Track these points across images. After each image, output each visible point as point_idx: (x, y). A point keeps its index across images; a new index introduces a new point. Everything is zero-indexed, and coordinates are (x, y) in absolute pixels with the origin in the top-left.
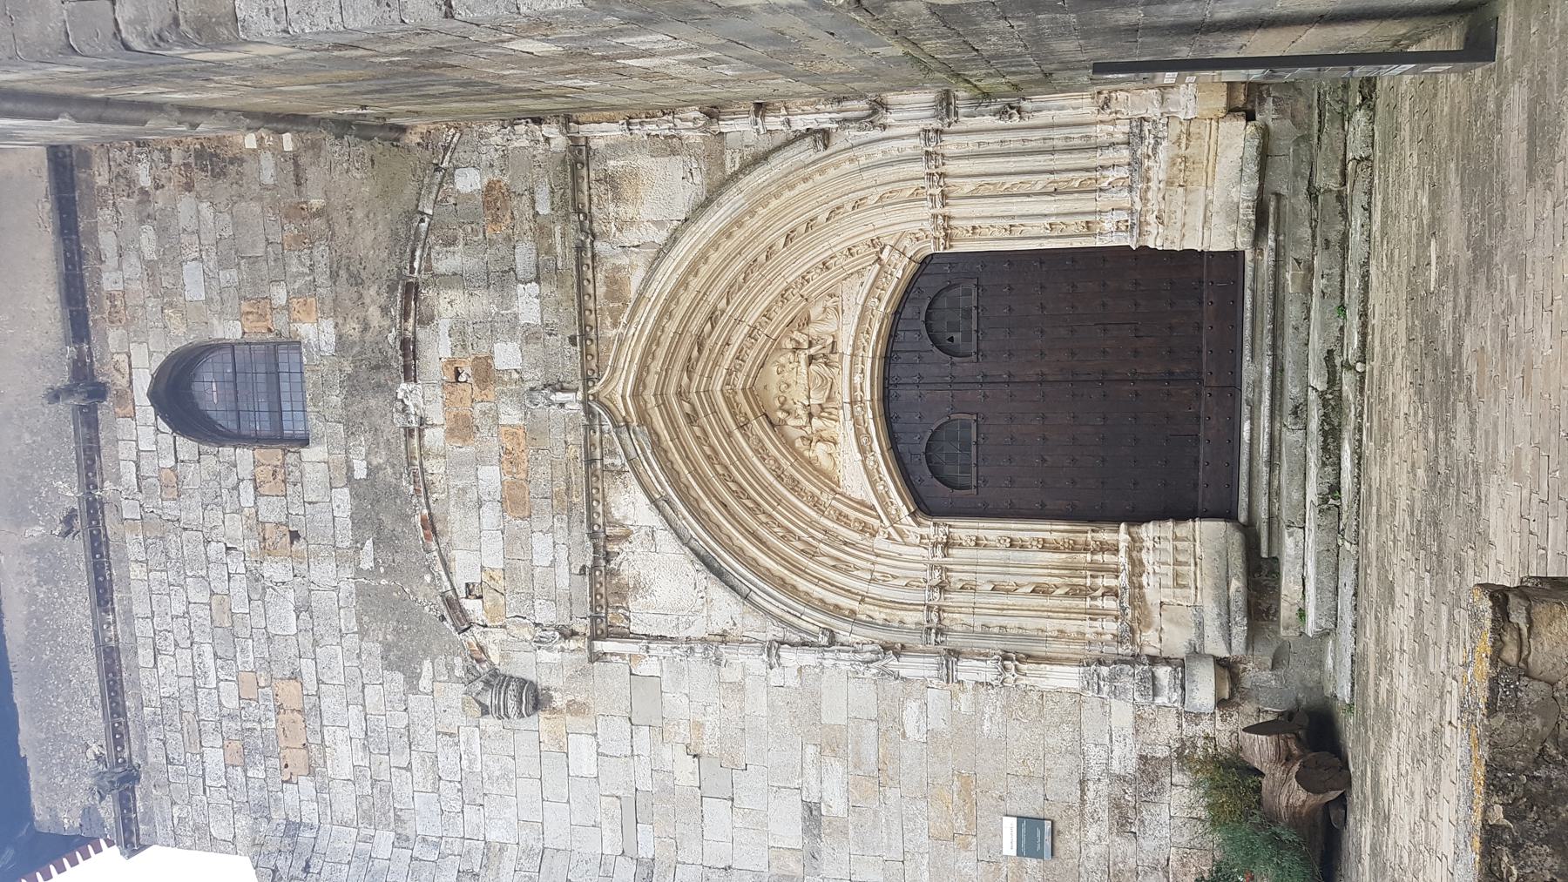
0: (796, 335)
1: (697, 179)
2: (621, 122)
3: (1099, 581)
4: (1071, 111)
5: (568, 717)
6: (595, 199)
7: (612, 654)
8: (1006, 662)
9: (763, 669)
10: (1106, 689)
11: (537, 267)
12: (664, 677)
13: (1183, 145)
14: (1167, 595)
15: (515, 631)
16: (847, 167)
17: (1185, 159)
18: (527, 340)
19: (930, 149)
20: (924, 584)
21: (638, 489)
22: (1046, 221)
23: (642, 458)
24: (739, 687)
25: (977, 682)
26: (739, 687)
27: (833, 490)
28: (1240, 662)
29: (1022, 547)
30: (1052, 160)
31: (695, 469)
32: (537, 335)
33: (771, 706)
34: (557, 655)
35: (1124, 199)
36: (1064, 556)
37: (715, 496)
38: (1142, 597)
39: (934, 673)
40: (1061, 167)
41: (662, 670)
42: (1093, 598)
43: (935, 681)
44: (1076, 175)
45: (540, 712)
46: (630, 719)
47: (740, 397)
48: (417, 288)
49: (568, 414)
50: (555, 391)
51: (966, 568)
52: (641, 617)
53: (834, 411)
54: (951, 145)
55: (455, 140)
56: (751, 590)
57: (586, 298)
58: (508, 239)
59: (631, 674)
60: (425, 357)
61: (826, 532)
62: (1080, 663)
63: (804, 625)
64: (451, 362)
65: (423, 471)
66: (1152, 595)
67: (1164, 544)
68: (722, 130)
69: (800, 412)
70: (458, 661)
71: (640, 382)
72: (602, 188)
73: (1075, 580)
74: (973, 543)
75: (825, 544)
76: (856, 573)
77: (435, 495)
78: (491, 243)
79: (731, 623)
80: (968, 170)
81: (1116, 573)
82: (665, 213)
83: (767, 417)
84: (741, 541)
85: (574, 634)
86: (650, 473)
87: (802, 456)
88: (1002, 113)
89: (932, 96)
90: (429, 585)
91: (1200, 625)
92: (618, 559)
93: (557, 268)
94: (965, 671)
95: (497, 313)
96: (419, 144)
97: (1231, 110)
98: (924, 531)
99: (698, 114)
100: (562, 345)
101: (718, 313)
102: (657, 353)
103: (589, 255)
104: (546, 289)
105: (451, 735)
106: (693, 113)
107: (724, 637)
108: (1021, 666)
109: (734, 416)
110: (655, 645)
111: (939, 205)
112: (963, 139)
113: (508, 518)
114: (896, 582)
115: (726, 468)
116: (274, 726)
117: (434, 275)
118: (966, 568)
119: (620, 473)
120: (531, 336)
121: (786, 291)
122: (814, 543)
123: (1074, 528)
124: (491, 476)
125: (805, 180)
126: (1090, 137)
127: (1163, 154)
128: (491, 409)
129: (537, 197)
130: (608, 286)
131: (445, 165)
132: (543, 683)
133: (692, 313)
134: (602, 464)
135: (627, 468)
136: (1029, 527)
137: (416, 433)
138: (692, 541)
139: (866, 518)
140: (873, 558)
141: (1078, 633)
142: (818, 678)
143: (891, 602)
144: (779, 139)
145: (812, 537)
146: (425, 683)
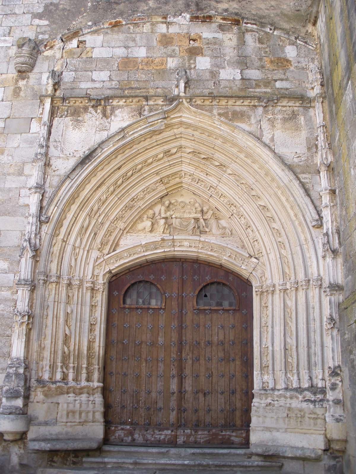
0: (211, 212)
1: (296, 160)
2: (324, 122)
3: (71, 371)
4: (331, 355)
5: (13, 88)
6: (284, 109)
7: (43, 109)
8: (27, 317)
9: (29, 186)
10: (11, 371)
11: (249, 79)
12: (29, 135)
13: (310, 416)
14: (63, 407)
15: (60, 62)
16: (302, 238)
17: (303, 417)
18: (211, 72)
19: (311, 282)
20: (71, 275)
21: (131, 122)
22: (269, 345)
23: (148, 125)
24: (20, 173)
25: (16, 301)
26: (20, 173)
27: (125, 229)
28: (24, 446)
29: (91, 330)
30: (304, 346)
31: (140, 153)
32: (214, 77)
33: (10, 190)
34: (45, 83)
35: (281, 385)
36: (85, 352)
37: (124, 163)
38: (62, 394)
39: (22, 277)
40: (300, 351)
41: (32, 133)
42: (62, 367)
43: (18, 278)
44: (295, 360)
45: (17, 74)
46: (9, 118)
47: (178, 180)
48: (237, 24)
49: (172, 90)
50: (186, 83)
51: (80, 299)
52: (62, 123)
53: (168, 231)
54: (314, 293)
55: (310, 47)
56: (73, 180)
57: (234, 101)
58: (263, 67)
59: (32, 118)
60: (203, 26)
61: (102, 224)
62: (26, 358)
63: (52, 208)
64: (200, 37)
65: (145, 23)
66: (62, 399)
67: (91, 406)
68: (321, 173)
69: (168, 214)
70: (47, 36)
71: (188, 126)
72: (290, 113)
73: (72, 358)
74: (93, 304)
75: (96, 223)
76: (79, 239)
77: (132, 28)
78: (261, 59)
79: (56, 169)
80: (299, 303)
81: (76, 379)
82: (278, 143)
83: (166, 195)
84: (100, 175)
85: (55, 90)
86: (140, 128)
87: (144, 213)
88: (332, 319)
89: (340, 282)
90: (86, 24)
91: (46, 424)
92: (93, 112)
93: (249, 88)
94: (23, 294)
95: (225, 60)
96: (307, 31)
97: (329, 442)
98: (101, 277)
99: (329, 160)
100: (209, 88)
101: (224, 169)
102: (203, 135)
103: (256, 104)
104: (238, 83)
105: (9, 33)
106: (330, 158)
107: (47, 165)
108: (25, 325)
109: (168, 176)
110: (46, 129)
111: (281, 288)
112: (317, 299)
113: (119, 60)
114: (73, 260)
115: (140, 171)
116: (110, 107)
117: (244, 33)
118: (80, 299)
119: (140, 114)
120: (214, 74)
121: (235, 206)
122: (96, 217)
123: (101, 359)
124: (141, 53)
125: (296, 215)
126: (316, 366)
127: (304, 405)
128: (176, 54)
129: (284, 82)
130: (240, 112)
131: (298, 42)
132: (32, 75)
133: (225, 155)
134: (145, 105)
135: (142, 117)
136: (102, 335)
137: (164, 20)
138: (101, 149)
139: (109, 246)
140: (87, 248)
141: (43, 357)
142: (23, 215)
143: (62, 257)
144: (317, 203)
145: (100, 216)
146: (37, 21)
